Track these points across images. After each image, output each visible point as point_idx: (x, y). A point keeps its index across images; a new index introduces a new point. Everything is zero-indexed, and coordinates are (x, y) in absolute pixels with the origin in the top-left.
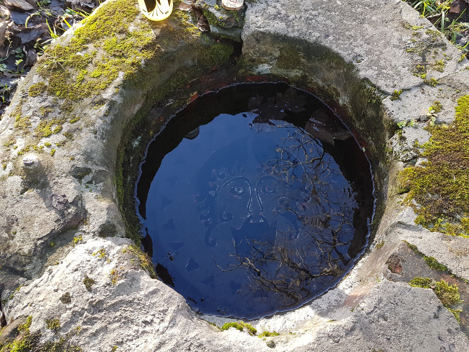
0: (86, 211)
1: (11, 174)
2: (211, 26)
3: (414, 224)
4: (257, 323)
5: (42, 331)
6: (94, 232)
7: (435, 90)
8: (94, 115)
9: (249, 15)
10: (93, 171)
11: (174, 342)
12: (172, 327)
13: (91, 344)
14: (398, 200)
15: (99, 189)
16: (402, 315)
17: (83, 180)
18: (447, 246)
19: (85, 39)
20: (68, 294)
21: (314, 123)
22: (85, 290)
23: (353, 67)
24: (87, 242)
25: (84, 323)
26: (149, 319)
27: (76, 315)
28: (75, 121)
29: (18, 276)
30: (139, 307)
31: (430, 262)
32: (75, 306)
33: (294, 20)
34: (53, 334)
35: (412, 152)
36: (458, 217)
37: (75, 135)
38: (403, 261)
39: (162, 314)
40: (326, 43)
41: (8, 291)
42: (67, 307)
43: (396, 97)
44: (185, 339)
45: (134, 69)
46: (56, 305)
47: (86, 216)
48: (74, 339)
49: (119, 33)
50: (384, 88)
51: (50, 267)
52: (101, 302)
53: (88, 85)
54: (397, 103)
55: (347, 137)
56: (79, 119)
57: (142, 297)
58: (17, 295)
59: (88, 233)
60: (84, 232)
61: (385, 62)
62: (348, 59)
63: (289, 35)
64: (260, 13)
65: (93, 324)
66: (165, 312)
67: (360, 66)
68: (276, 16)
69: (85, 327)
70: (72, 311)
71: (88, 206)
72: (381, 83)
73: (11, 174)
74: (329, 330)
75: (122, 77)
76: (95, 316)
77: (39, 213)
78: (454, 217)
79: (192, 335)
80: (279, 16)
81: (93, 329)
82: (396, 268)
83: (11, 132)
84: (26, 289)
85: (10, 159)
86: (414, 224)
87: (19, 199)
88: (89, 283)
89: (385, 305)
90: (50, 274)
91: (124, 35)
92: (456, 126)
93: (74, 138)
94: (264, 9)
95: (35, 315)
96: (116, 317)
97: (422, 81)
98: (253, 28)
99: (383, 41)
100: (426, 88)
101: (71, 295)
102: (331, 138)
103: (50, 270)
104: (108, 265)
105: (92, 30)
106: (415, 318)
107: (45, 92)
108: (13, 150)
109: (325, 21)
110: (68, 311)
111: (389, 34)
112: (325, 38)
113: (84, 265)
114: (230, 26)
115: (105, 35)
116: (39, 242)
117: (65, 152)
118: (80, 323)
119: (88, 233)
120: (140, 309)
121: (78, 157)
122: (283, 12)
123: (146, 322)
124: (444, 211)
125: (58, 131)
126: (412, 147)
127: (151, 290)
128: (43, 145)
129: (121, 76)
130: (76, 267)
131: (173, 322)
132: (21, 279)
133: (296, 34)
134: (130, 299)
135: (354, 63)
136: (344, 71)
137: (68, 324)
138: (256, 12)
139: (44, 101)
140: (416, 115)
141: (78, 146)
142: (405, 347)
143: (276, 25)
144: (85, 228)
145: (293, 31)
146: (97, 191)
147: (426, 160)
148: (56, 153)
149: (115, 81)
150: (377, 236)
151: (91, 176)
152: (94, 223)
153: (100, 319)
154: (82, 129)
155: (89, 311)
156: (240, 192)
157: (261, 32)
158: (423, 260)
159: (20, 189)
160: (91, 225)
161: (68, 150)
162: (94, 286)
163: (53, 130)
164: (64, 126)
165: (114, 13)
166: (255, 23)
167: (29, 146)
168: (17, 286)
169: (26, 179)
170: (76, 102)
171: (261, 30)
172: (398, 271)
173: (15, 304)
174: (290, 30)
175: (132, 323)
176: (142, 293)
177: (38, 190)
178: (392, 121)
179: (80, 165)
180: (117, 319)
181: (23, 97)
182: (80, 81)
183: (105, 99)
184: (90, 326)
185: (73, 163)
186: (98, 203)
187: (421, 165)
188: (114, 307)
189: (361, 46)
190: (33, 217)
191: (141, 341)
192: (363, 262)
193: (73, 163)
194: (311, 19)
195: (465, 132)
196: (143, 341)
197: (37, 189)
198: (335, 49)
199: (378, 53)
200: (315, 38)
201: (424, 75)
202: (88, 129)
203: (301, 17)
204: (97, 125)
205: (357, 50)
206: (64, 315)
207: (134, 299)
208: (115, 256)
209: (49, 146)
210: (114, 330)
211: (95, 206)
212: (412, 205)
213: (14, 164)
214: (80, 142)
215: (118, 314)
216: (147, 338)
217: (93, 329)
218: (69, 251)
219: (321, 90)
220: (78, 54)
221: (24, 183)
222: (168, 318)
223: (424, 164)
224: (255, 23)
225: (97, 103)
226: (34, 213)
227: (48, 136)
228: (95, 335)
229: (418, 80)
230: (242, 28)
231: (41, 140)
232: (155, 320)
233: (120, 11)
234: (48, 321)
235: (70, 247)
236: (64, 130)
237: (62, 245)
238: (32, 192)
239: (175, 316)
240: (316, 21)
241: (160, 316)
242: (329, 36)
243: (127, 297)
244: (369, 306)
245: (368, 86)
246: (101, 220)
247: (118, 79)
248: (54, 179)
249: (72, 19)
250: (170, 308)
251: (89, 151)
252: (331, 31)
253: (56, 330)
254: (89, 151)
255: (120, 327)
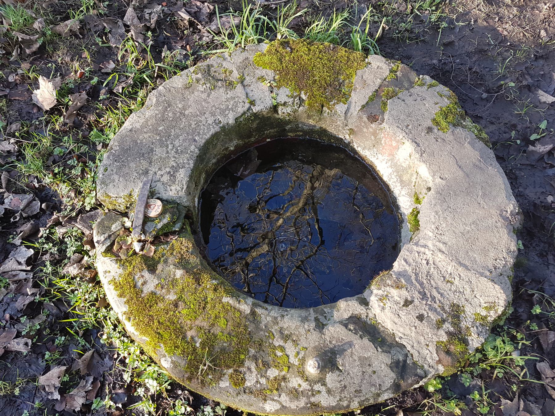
0: (351, 317)
1: (324, 384)
2: (174, 229)
3: (346, 106)
4: (404, 214)
5: (446, 331)
6: (366, 309)
7: (247, 78)
8: (266, 318)
9: (169, 196)
10: (316, 316)
11: (438, 243)
12: (428, 247)
13: (448, 296)
14: (325, 115)
15: (330, 311)
16: (405, 117)
17: (324, 323)
18: (361, 89)
19: (181, 340)
20: (417, 317)
21: (242, 173)
22: (413, 304)
23: (224, 127)
24: (374, 313)
25: (435, 302)
26: (425, 262)
27: (431, 308)
28: (273, 334)
29: (407, 365)
30: (418, 269)
31: (371, 99)
32: (425, 310)
33: (177, 163)
34: (446, 323)
35: (296, 99)
36: (341, 81)
37: (286, 332)
38: (372, 113)
39: (420, 254)
40: (201, 141)
41: (419, 371)
42: (426, 316)
43: (252, 103)
44: (434, 238)
45: (220, 289)
46: (426, 324)
47: (354, 317)
48: (447, 308)
49: (176, 307)
50: (245, 109)
51: (397, 339)
52: (420, 293)
53: (235, 329)
54: (258, 102)
55: (256, 151)
56: (271, 331)
57: (410, 268)
58: (420, 363)
59: (367, 313)
60: (367, 316)
61: (222, 105)
62: (217, 129)
63: (192, 167)
64: (166, 187)
65: (435, 297)
66: (418, 253)
67: (224, 121)
68: (171, 175)
69: (438, 302)
70: (429, 312)
71: (346, 316)
72: (241, 110)
73: (324, 384)
74: (417, 156)
75: (229, 298)
76: (429, 296)
77: (357, 354)
78: (341, 83)
79: (431, 234)
80: (172, 173)
81: (437, 296)
82: (375, 118)
83: (283, 395)
84: (416, 355)
85: (310, 388)
86: (346, 106)
87: (347, 373)
88: (407, 303)
89: (400, 124)
90: (402, 338)
91: (180, 303)
92: (278, 70)
93: (289, 333)
94: (163, 184)
95: (435, 339)
96: (427, 283)
97: (239, 84)
98: (182, 194)
99: (203, 103)
100: (245, 83)
101: (417, 315)
102: (257, 162)
103: (399, 338)
104: (391, 293)
105: (171, 334)
106: (406, 111)
107: (240, 370)
108: (302, 387)
109: (179, 140)
110: (429, 315)
111: (197, 98)
112: (197, 142)
113: (394, 310)
114: (177, 212)
115: (177, 321)
116: (379, 350)
117: (302, 338)
118: (436, 306)
119: (367, 313)
120: (419, 268)
121: (306, 326)
122: (168, 170)
123: (427, 264)
124: (338, 88)
125: (282, 349)
126: (292, 99)
127: (405, 264)
128: (297, 360)
129: (227, 299)
130: (397, 316)
131: (425, 246)
132: (408, 362)
133: (192, 162)
134: (414, 274)
135: (221, 125)
136: (223, 135)
137: (438, 314)
138: (166, 190)
139: (249, 369)
140: (267, 93)
141: (297, 328)
142: (422, 118)
143: (182, 176)
144: (364, 316)
145: (189, 164)
146: (332, 312)
147: (302, 92)
148: (304, 346)
149: (232, 304)
150: (340, 136)
151: (320, 317)
152: (359, 310)
153: (430, 292)
154: (281, 327)
155: (427, 300)
156: (284, 246)
157: (187, 188)
158: (370, 103)
159: (338, 372)
160: (361, 312)
161: (301, 336)
162: (409, 299)
163: (281, 354)
164: (277, 344)
165: (150, 316)
166: (178, 192)
167: (298, 372)
168: (414, 363)
169: (329, 368)
170: (252, 337)
171: (185, 187)
172: (377, 117)
173: (427, 363)
174: (187, 166)
175: (429, 272)
176: (407, 268)
177: (337, 357)
178: (271, 108)
179: (313, 325)
180: (428, 282)
181: (245, 392)
182: (230, 337)
183: (251, 310)
184: (436, 299)
185: (312, 331)
186: (342, 309)
187: (306, 96)
188: (421, 284)
189: (206, 118)
190: (360, 358)
191: (440, 265)
192: (358, 147)
193: (312, 331)
194: (178, 150)
195: (283, 66)
196: (440, 263)
197: (337, 358)
198: (208, 136)
199: (214, 108)
200: (196, 149)
201: (235, 82)
202: (280, 322)
203: (174, 157)
204: (276, 315)
205: (210, 122)
206: (432, 317)
207: (413, 273)
208: (384, 290)
209: (298, 353)
210: (436, 283)
211: (345, 310)
212: (334, 105)
213: (315, 383)
214: (293, 326)
215: (425, 282)
216: (437, 262)
217: (437, 296)
218: (383, 327)
219: (218, 161)
220: (198, 345)
221: (332, 371)
222: (422, 249)
223: (306, 94)
224: (178, 191)
225: (254, 318)
226: (356, 358)
227: (288, 356)
228: (442, 295)
229: (239, 87)
230: (178, 204)
231: (292, 363)
232: (424, 258)
233: (149, 311)
234: (438, 328)
235: (380, 326)
236: (281, 343)
237: (379, 333)
238: (340, 361)
239: (420, 246)
240: (179, 147)
241: (422, 255)
242: (195, 139)
243: (413, 277)
244: (402, 133)
245: (241, 119)
246: (356, 305)
247: (231, 302)
248: (328, 344)
249: (112, 396)
250: (415, 250)
251: (300, 319)
252: (190, 137)
253: (443, 321)
254: (300, 319)
255: (433, 279)
